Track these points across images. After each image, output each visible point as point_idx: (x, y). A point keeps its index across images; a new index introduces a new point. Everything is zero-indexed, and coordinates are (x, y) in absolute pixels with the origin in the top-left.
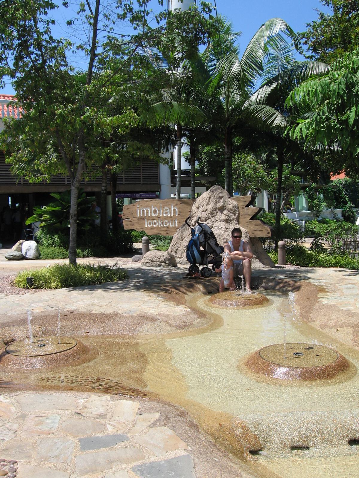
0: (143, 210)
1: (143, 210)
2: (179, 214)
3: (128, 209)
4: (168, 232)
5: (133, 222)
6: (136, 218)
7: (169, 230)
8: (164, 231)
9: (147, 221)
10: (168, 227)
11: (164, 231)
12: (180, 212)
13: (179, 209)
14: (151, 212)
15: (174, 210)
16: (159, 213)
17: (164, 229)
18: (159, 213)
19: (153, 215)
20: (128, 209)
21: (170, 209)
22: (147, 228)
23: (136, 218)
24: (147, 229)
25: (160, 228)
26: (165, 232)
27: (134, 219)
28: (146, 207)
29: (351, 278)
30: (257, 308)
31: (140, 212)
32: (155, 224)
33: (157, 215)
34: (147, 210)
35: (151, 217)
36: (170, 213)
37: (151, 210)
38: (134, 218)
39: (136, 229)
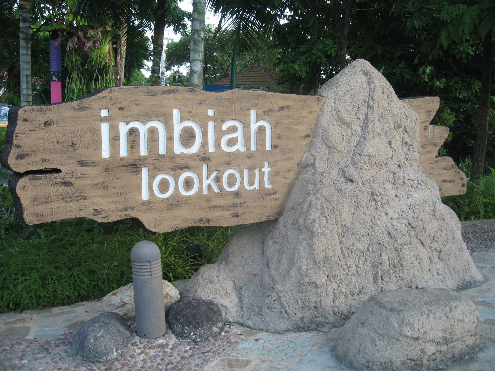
0: (133, 132)
1: (133, 132)
2: (275, 146)
3: (47, 124)
4: (240, 210)
5: (78, 183)
6: (94, 164)
7: (241, 204)
8: (222, 208)
9: (152, 177)
10: (237, 194)
11: (222, 208)
12: (277, 137)
13: (275, 126)
14: (170, 139)
15: (261, 130)
16: (205, 144)
17: (229, 201)
18: (205, 144)
19: (178, 149)
20: (47, 124)
21: (247, 126)
22: (149, 205)
23: (94, 164)
24: (150, 209)
25: (208, 199)
26: (227, 213)
27: (80, 170)
28: (145, 117)
29: (119, 213)
30: (208, 221)
31: (115, 139)
32: (188, 184)
33: (194, 149)
34: (153, 132)
35: (171, 156)
36: (247, 139)
37: (169, 129)
38: (83, 164)
39: (97, 212)
